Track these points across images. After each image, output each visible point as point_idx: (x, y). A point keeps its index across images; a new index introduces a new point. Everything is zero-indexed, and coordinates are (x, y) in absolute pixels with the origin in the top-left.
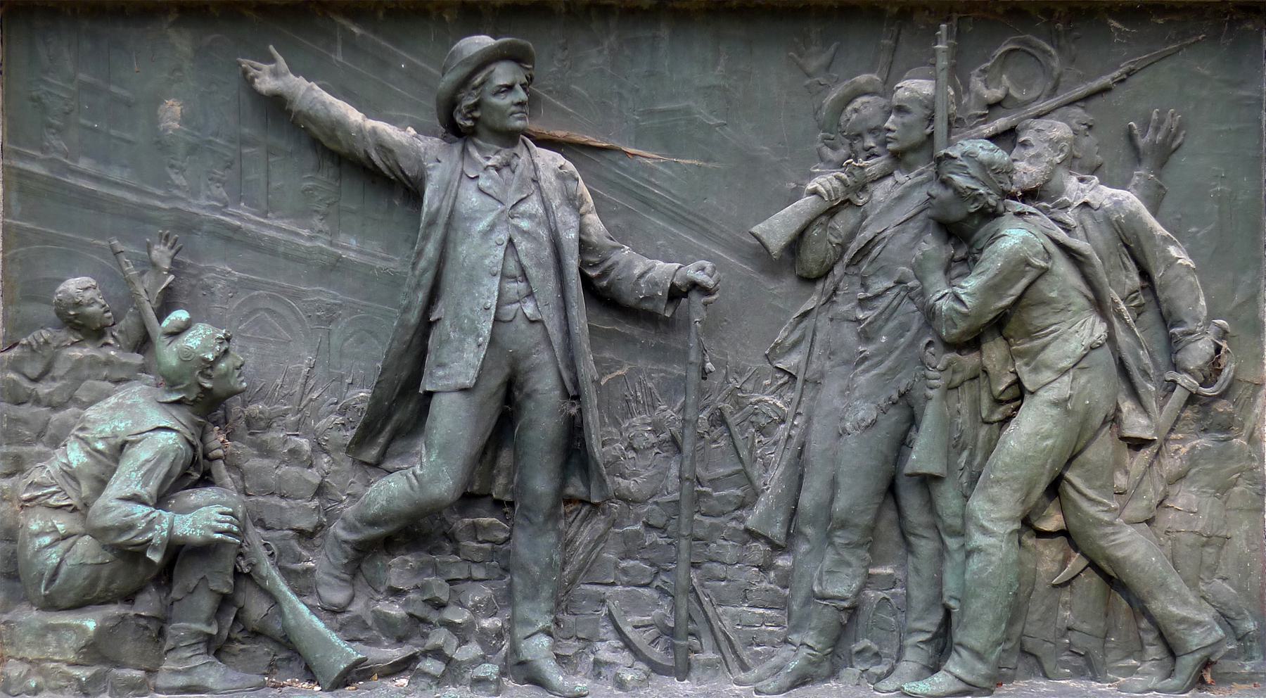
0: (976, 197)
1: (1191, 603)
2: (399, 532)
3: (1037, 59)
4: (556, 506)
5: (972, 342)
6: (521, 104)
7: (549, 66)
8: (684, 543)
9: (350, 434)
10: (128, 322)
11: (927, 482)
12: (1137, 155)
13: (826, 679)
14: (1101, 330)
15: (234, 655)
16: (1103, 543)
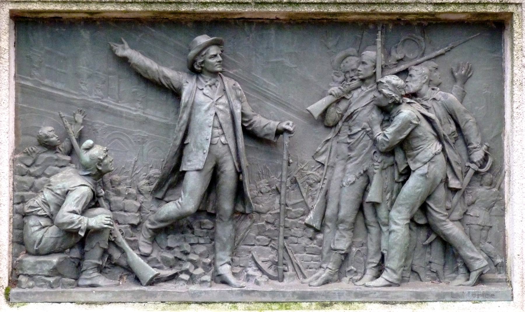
0: (392, 98)
1: (475, 252)
2: (172, 225)
3: (416, 42)
4: (232, 215)
5: (390, 152)
6: (220, 62)
7: (228, 46)
8: (281, 229)
9: (153, 187)
10: (65, 144)
11: (375, 205)
12: (455, 79)
13: (336, 281)
14: (439, 147)
15: (106, 273)
16: (442, 228)
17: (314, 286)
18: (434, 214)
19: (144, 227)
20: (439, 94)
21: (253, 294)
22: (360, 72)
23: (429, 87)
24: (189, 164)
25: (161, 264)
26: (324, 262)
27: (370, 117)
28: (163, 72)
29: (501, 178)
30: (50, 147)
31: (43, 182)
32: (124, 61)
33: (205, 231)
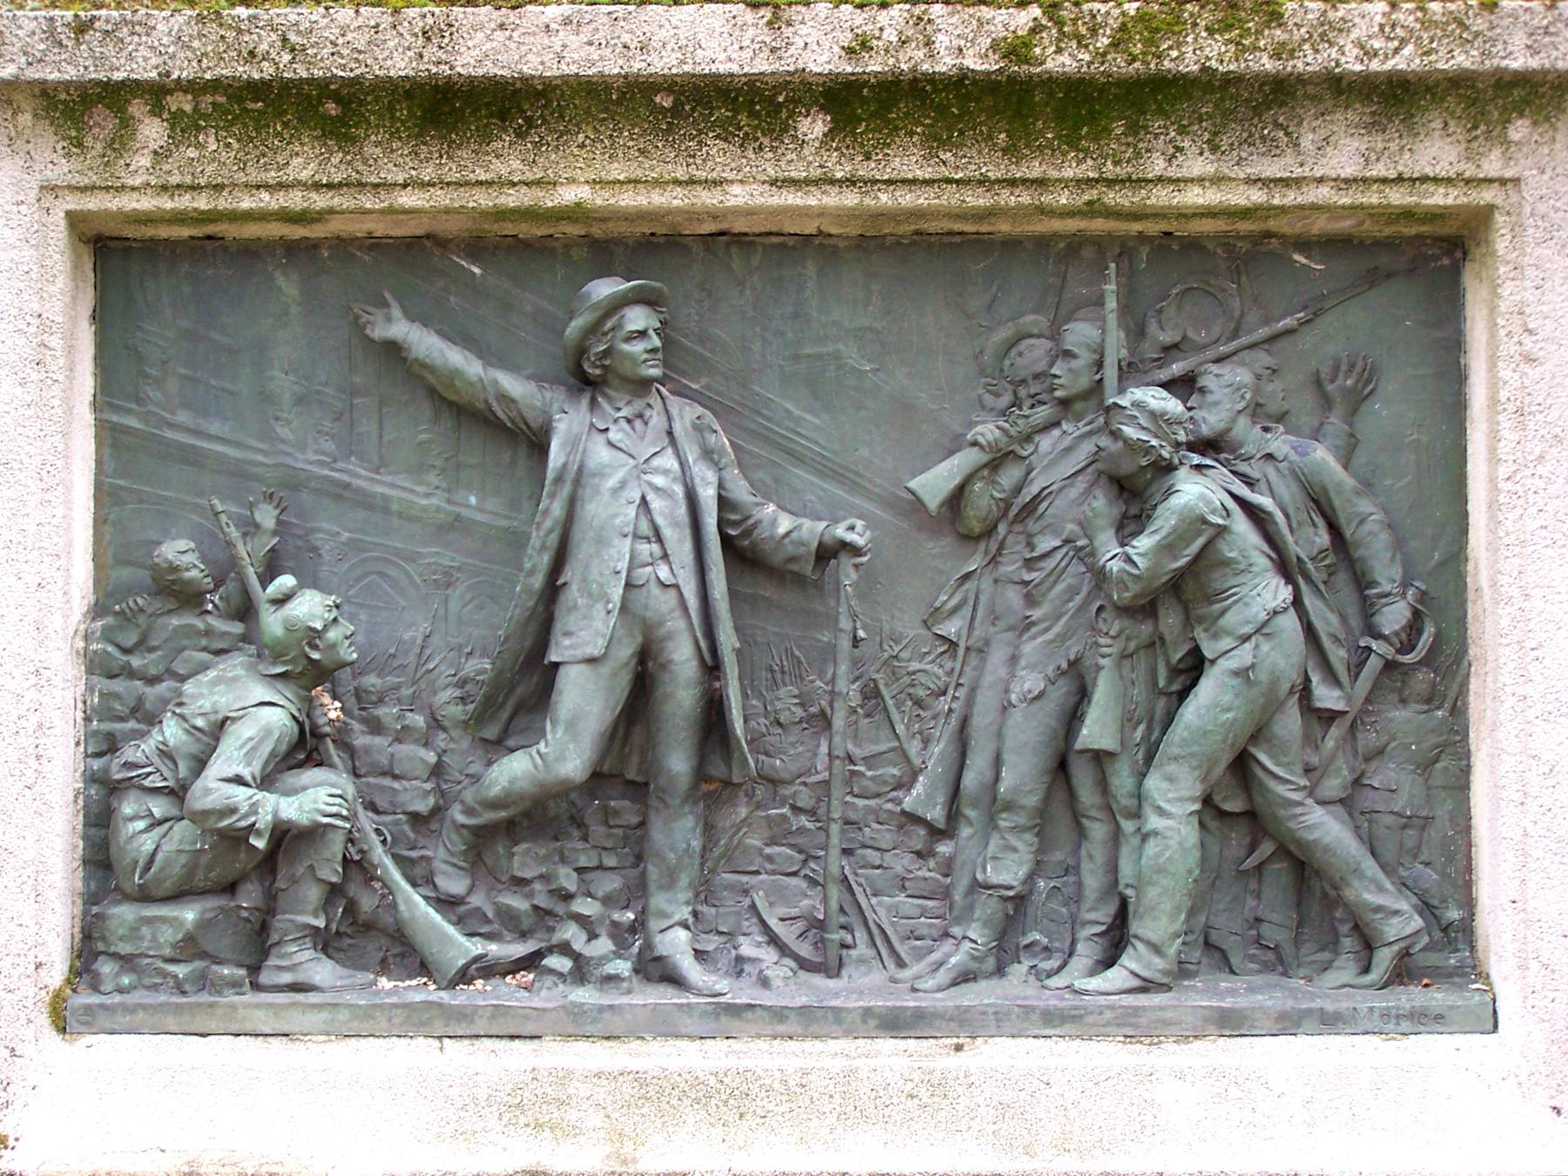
2: (527, 814)
4: (695, 786)
5: (1145, 608)
6: (654, 351)
8: (835, 828)
11: (1100, 758)
12: (1326, 402)
13: (989, 976)
14: (1286, 593)
16: (1292, 825)
17: (925, 992)
18: (1272, 784)
19: (448, 823)
20: (1280, 443)
21: (749, 1015)
22: (1056, 381)
23: (1254, 423)
24: (567, 642)
25: (496, 926)
26: (958, 921)
27: (1085, 507)
28: (496, 382)
29: (1459, 679)
30: (187, 597)
31: (169, 695)
32: (393, 350)
33: (619, 831)
